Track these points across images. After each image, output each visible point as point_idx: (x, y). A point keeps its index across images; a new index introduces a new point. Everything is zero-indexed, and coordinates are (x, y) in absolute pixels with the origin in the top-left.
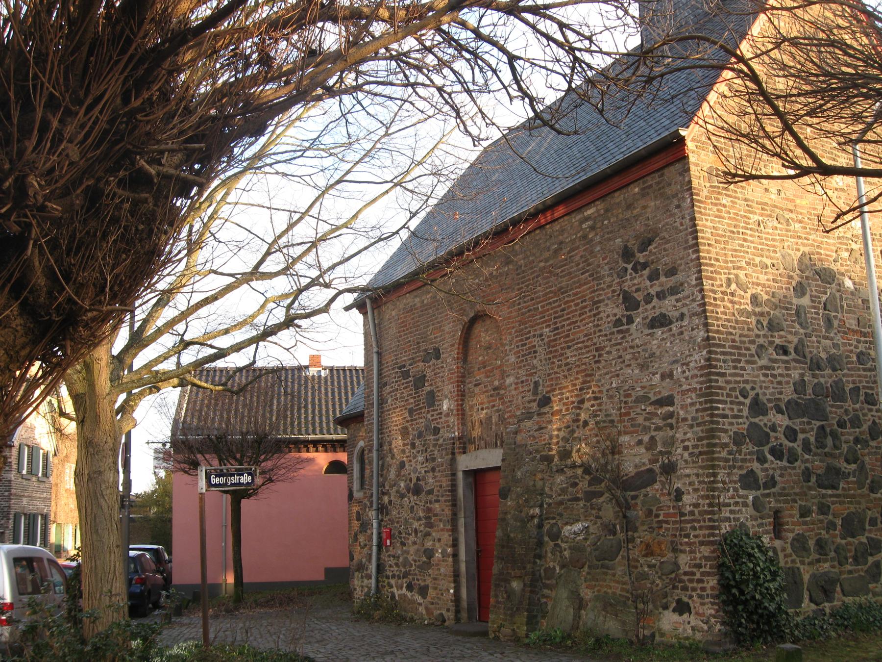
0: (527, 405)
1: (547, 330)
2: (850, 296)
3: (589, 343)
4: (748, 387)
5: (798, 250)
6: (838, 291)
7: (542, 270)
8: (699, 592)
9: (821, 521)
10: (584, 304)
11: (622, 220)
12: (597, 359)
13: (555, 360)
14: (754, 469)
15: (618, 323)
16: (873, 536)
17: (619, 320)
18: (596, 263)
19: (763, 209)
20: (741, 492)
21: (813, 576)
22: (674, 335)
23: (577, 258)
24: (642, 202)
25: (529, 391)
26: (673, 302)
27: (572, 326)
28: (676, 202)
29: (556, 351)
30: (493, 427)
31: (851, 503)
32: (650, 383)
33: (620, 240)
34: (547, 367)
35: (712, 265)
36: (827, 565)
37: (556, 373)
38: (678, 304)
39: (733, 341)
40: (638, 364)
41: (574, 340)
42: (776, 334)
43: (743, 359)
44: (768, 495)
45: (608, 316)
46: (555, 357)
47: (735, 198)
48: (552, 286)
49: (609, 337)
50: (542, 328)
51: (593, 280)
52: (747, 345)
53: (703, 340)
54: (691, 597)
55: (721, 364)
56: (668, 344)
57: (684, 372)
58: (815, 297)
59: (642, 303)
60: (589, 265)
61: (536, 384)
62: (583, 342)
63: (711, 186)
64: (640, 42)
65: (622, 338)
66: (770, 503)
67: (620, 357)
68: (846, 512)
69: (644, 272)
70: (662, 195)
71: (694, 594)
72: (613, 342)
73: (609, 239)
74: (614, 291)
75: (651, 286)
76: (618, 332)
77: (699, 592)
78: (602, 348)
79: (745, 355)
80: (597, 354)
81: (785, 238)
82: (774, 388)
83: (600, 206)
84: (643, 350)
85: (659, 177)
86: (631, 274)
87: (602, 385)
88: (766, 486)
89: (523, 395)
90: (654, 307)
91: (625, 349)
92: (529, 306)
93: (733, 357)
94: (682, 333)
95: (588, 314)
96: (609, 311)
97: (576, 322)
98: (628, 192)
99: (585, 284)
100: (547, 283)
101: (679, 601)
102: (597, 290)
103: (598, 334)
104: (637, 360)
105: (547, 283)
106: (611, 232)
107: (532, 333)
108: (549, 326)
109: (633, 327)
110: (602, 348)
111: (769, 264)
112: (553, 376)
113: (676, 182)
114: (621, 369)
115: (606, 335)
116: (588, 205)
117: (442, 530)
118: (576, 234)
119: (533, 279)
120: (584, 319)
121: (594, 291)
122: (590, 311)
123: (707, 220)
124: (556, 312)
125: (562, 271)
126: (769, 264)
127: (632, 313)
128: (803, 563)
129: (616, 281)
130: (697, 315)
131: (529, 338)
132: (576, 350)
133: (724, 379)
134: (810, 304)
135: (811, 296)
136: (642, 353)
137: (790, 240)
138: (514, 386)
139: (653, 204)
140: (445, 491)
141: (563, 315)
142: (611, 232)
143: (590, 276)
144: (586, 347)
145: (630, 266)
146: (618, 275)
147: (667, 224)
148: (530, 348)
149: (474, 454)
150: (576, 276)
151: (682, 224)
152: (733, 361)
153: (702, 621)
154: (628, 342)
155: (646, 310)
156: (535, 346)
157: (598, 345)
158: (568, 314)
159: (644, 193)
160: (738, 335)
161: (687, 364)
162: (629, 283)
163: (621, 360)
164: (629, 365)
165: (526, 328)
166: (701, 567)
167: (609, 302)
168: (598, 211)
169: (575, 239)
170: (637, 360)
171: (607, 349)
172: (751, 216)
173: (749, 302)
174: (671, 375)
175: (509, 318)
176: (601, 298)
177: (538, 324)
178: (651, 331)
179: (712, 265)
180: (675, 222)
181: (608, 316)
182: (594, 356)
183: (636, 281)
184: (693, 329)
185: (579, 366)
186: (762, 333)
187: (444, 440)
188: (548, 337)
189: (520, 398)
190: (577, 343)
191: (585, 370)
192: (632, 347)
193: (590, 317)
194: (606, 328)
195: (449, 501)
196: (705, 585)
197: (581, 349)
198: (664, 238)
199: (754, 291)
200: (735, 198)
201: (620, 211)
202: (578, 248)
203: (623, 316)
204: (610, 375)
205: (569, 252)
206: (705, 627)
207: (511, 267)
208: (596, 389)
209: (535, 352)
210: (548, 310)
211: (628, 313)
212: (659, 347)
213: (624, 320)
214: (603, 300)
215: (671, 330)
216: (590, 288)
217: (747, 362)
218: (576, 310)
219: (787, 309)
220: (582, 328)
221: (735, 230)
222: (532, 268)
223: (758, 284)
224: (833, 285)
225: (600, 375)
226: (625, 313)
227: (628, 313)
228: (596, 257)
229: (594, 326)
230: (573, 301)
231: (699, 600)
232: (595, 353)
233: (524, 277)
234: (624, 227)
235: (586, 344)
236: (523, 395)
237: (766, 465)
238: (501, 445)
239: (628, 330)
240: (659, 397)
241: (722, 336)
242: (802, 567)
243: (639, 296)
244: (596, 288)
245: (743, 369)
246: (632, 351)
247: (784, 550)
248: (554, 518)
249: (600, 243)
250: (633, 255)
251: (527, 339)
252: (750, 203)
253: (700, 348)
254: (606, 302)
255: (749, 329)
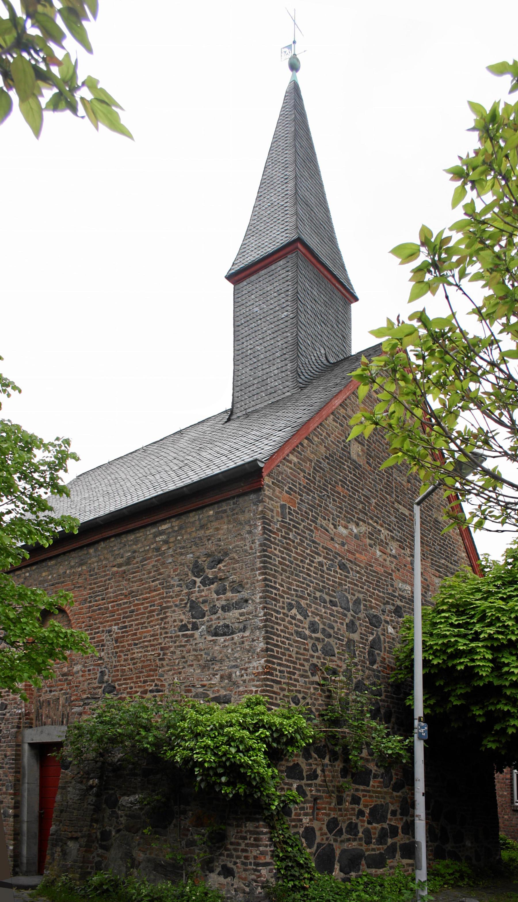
0: (92, 691)
1: (116, 627)
2: (391, 641)
3: (155, 642)
4: (300, 696)
5: (354, 595)
6: (383, 635)
7: (114, 574)
8: (243, 859)
9: (353, 809)
10: (153, 608)
11: (195, 538)
12: (161, 657)
13: (122, 654)
14: (300, 763)
15: (184, 628)
16: (392, 823)
17: (185, 626)
18: (167, 573)
19: (327, 553)
20: (287, 780)
21: (343, 851)
22: (235, 644)
23: (149, 567)
24: (216, 524)
25: (95, 679)
26: (237, 615)
27: (140, 626)
28: (247, 528)
29: (123, 646)
30: (60, 707)
31: (377, 797)
32: (210, 682)
33: (191, 555)
34: (113, 659)
35: (275, 588)
36: (354, 843)
37: (122, 665)
38: (241, 618)
39: (290, 656)
40: (200, 665)
41: (141, 638)
42: (328, 658)
43: (297, 672)
44: (310, 785)
45: (175, 621)
46: (121, 651)
47: (304, 537)
48: (122, 590)
49: (173, 639)
50: (111, 626)
51: (163, 588)
52: (302, 662)
53: (262, 651)
54: (235, 863)
55: (278, 673)
56: (230, 651)
57: (242, 676)
58: (364, 635)
59: (208, 613)
60: (160, 574)
61: (102, 673)
62: (150, 641)
63: (282, 521)
64: (230, 407)
65: (186, 641)
66: (311, 791)
67: (184, 657)
68: (374, 804)
69: (212, 586)
70: (235, 520)
71: (238, 861)
72: (178, 644)
73: (182, 554)
74: (182, 600)
75: (218, 599)
76: (183, 635)
77: (243, 859)
78: (168, 648)
79: (299, 670)
80: (162, 653)
81: (343, 582)
82: (322, 700)
83: (176, 523)
84: (205, 654)
85: (234, 504)
86: (199, 587)
87: (165, 680)
88: (309, 778)
89: (89, 681)
90: (218, 618)
91: (189, 652)
92: (100, 605)
93: (288, 670)
94: (243, 643)
95: (156, 617)
96: (175, 616)
97: (144, 623)
98: (203, 513)
99: (155, 590)
100: (118, 586)
101: (224, 867)
102: (166, 597)
103: (164, 636)
104: (199, 661)
105: (118, 586)
106: (183, 548)
107: (101, 629)
108: (117, 624)
109: (197, 634)
110: (168, 648)
111: (328, 600)
112: (119, 668)
113: (249, 511)
114: (184, 668)
115: (171, 637)
116: (163, 521)
117: (5, 793)
118: (149, 546)
119: (105, 581)
120: (152, 621)
121: (163, 598)
122: (158, 615)
123: (275, 549)
124: (126, 612)
125: (133, 577)
126: (328, 600)
127: (198, 621)
128: (335, 841)
129: (185, 591)
130: (259, 629)
131: (98, 632)
132: (143, 647)
133: (278, 686)
134: (359, 639)
135: (361, 634)
136: (204, 656)
137: (348, 585)
138: (81, 673)
139: (226, 527)
140: (10, 759)
141: (132, 616)
142: (183, 548)
143: (160, 584)
144: (152, 645)
145: (198, 580)
146: (187, 587)
147: (237, 546)
148: (98, 642)
149: (40, 729)
150: (146, 583)
151: (251, 548)
152: (289, 673)
153: (245, 884)
154: (192, 645)
155: (211, 620)
156: (103, 640)
157: (163, 645)
158: (137, 615)
159: (217, 517)
160: (295, 652)
161: (246, 669)
162: (197, 594)
163: (184, 660)
164: (192, 665)
165: (96, 624)
166: (247, 839)
167: (176, 609)
168: (172, 527)
169: (148, 550)
170: (199, 661)
171: (172, 649)
172: (316, 556)
173: (307, 626)
174: (230, 677)
175: (80, 613)
176: (169, 604)
177: (108, 621)
178: (214, 638)
179: (275, 588)
180: (245, 545)
181: (175, 621)
182: (159, 654)
183: (203, 594)
184: (253, 640)
185: (143, 661)
186: (316, 654)
187: (11, 715)
188: (117, 633)
189: (86, 683)
190: (144, 642)
191: (149, 665)
192: (195, 650)
193: (157, 620)
194: (173, 631)
195: (12, 768)
196: (249, 854)
197: (147, 646)
198: (234, 559)
199: (312, 620)
200: (304, 537)
201: (194, 529)
202: (150, 558)
203: (188, 622)
204: (173, 672)
205: (142, 561)
206: (247, 889)
207: (84, 568)
208: (159, 683)
209: (103, 645)
210: (118, 610)
211: (194, 620)
212: (221, 653)
213: (190, 626)
214: (171, 607)
215: (233, 639)
216: (159, 594)
217: (302, 676)
218: (144, 613)
219: (339, 639)
220: (149, 629)
221: (301, 564)
222: (105, 571)
223: (317, 615)
224: (379, 629)
225: (164, 671)
226: (191, 620)
227: (194, 620)
228: (167, 568)
229: (161, 628)
230: (143, 604)
231: (243, 867)
232: (160, 652)
233: (96, 578)
234: (196, 545)
235: (152, 643)
236: (89, 681)
237: (310, 761)
238: (67, 723)
239: (192, 636)
240: (217, 695)
241: (280, 650)
242: (334, 844)
243: (206, 608)
244: (165, 595)
245: (296, 680)
246: (195, 653)
247: (321, 829)
248: (113, 789)
249: (172, 556)
250: (203, 570)
251: (96, 633)
252: (317, 546)
253: (258, 658)
254: (174, 608)
255: (305, 649)
